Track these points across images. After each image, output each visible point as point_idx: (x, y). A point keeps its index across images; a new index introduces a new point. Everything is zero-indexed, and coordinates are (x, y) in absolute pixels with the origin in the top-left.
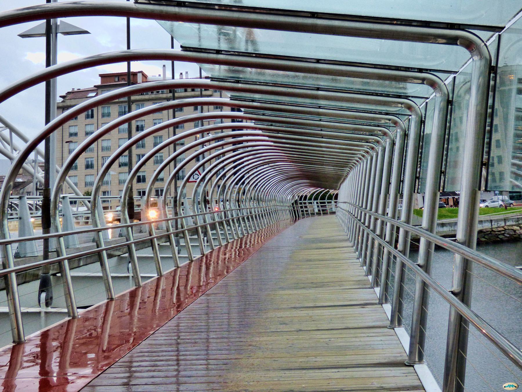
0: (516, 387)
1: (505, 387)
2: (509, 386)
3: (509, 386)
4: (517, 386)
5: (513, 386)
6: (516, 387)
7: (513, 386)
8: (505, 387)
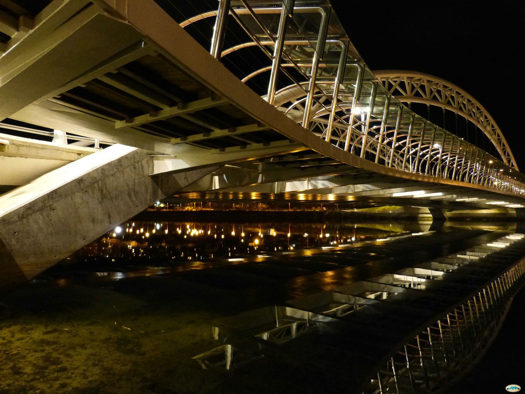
0: (519, 389)
1: (508, 389)
3: (512, 388)
5: (516, 388)
6: (519, 389)
7: (516, 388)
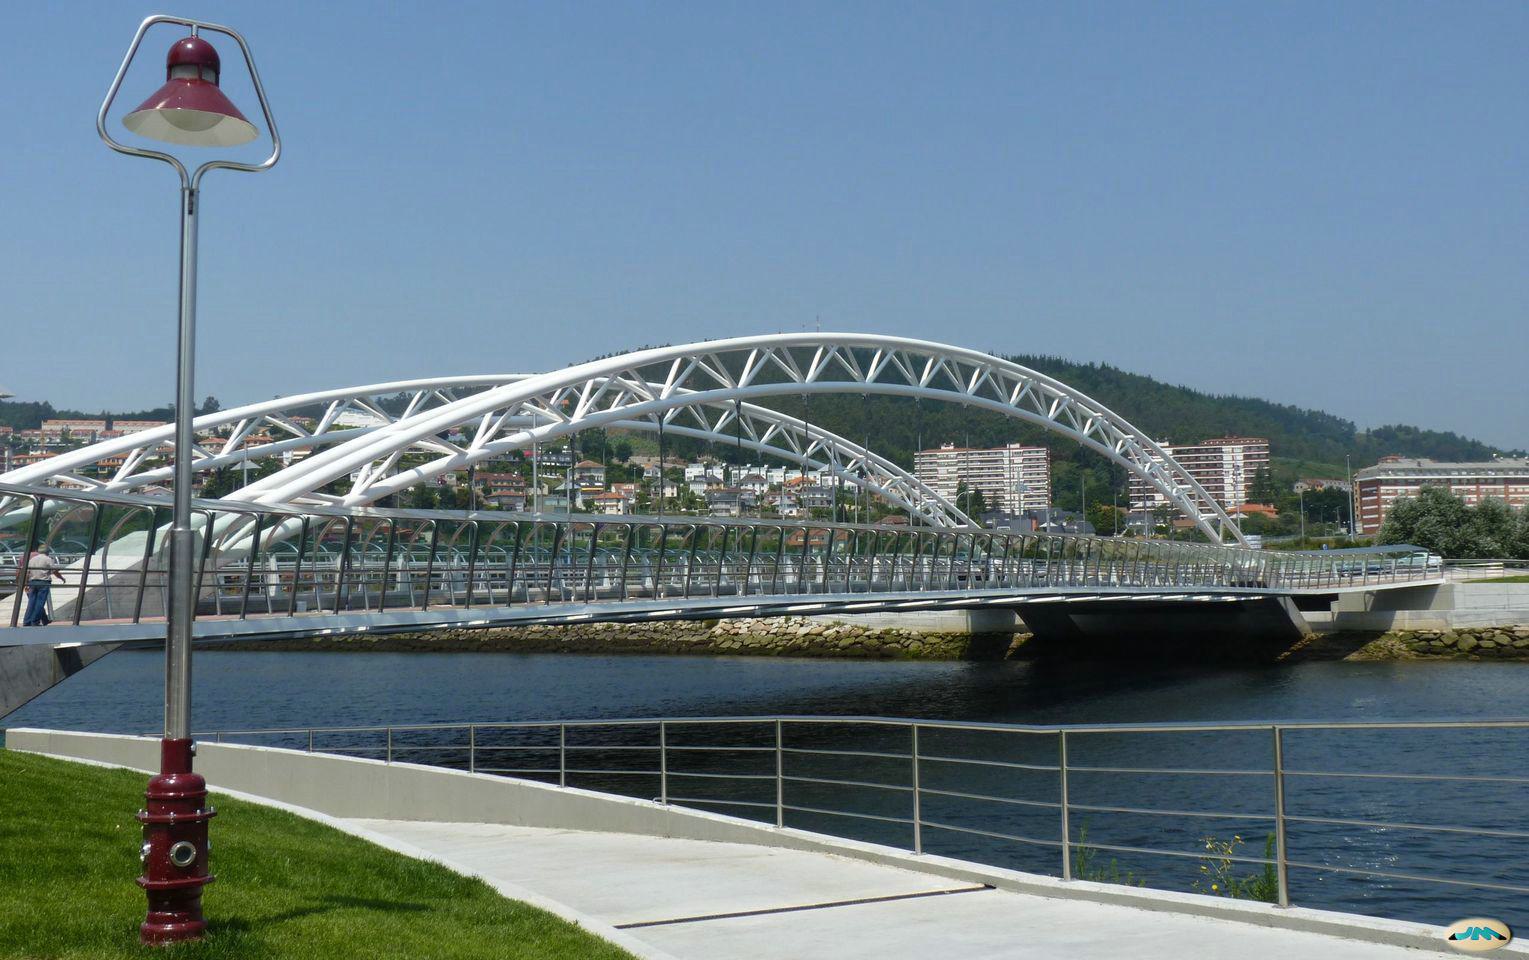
0: (1501, 938)
6: (1501, 938)
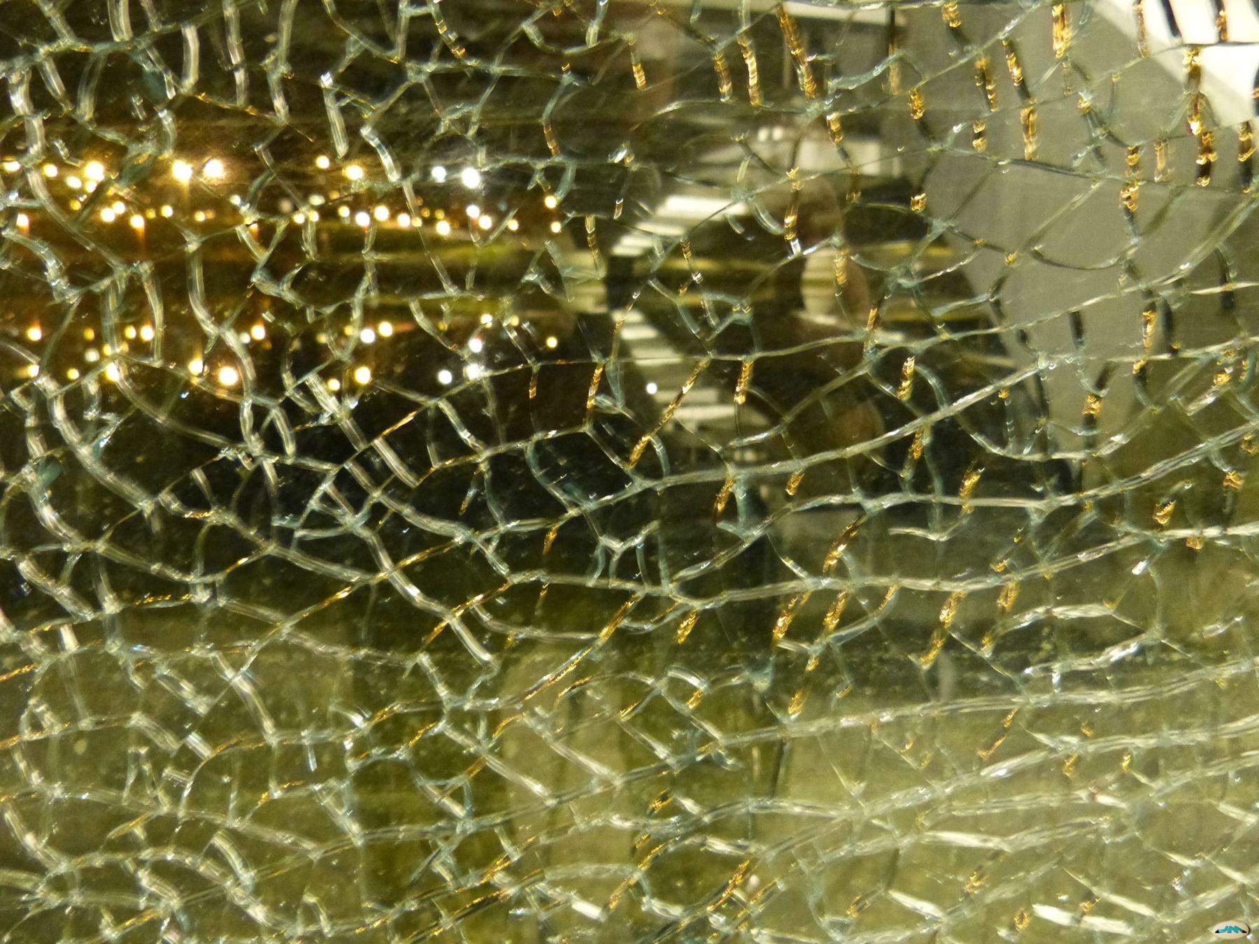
0: (1244, 932)
1: (1217, 932)
2: (1229, 930)
3: (1229, 930)
4: (1247, 930)
6: (1244, 932)
7: (1237, 929)
8: (1217, 932)
